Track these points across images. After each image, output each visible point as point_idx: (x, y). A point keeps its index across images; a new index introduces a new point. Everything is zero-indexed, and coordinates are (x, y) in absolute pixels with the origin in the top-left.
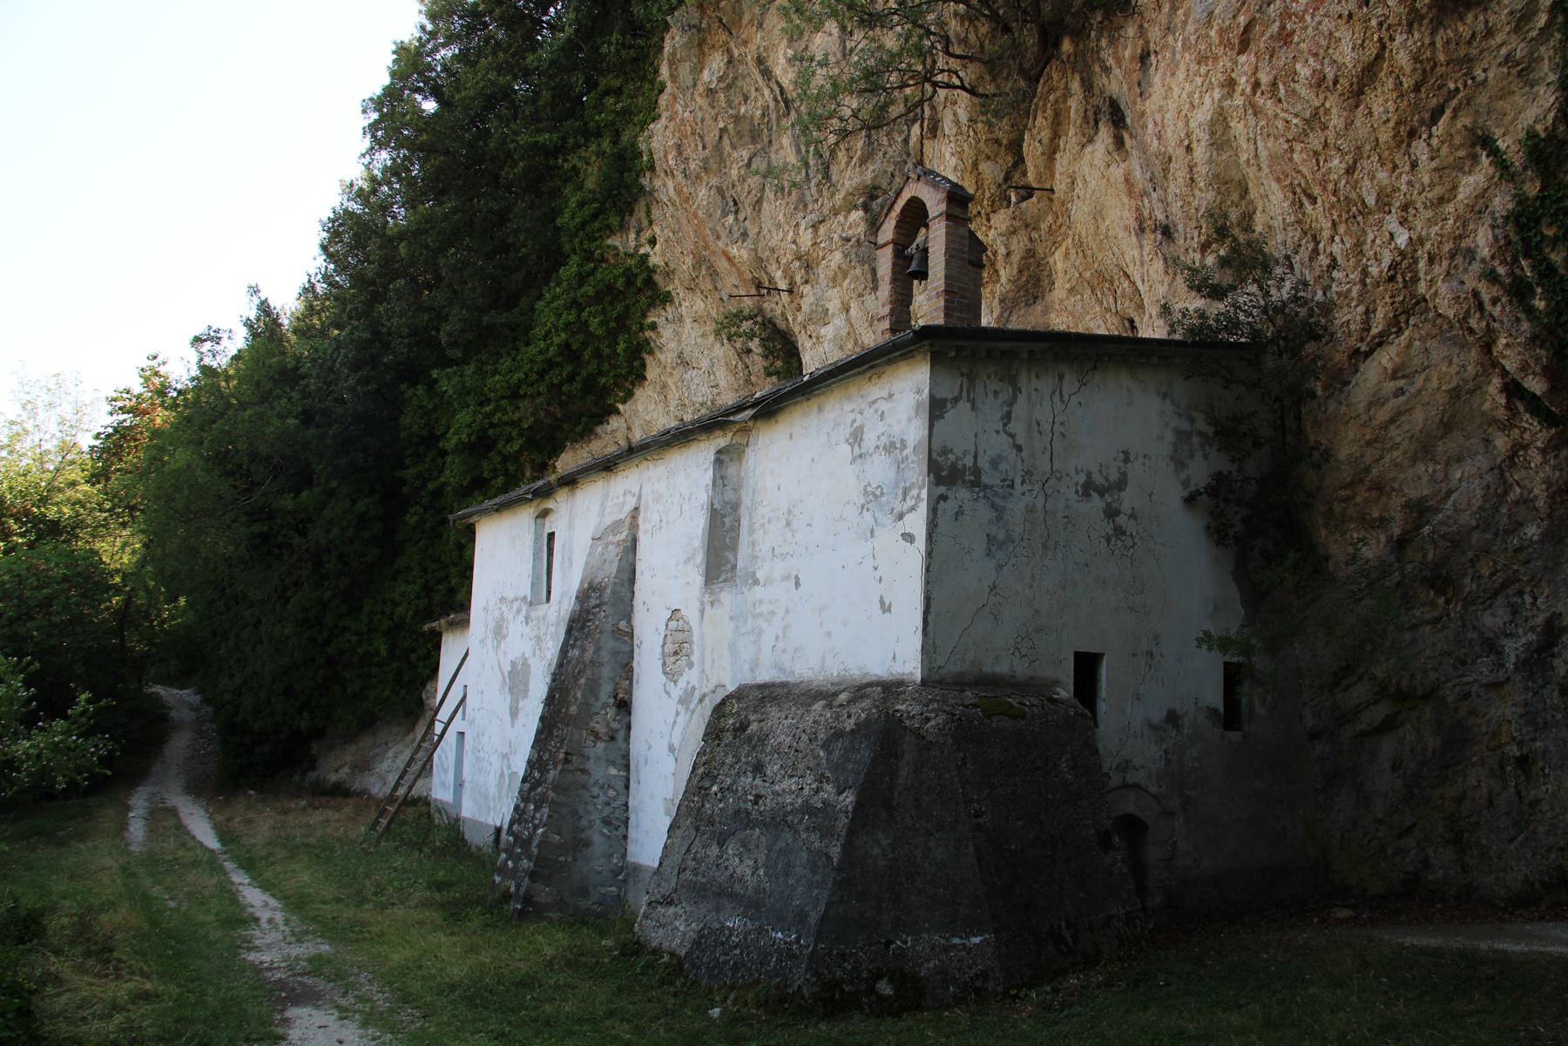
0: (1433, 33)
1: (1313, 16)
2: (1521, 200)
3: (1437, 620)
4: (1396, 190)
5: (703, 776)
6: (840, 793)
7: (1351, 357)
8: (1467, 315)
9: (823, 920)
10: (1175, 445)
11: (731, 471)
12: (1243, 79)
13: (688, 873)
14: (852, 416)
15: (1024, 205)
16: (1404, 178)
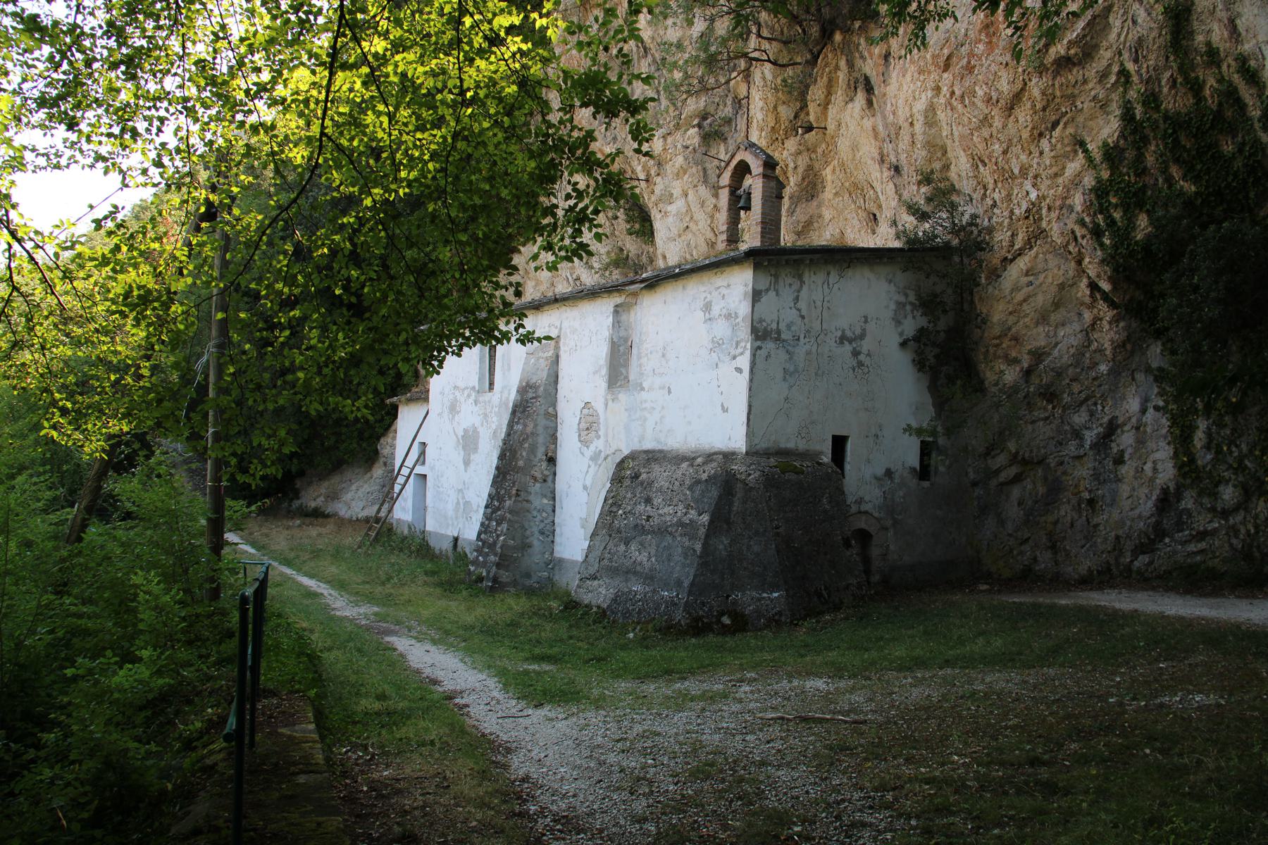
0: (1054, 79)
1: (986, 59)
2: (1099, 180)
3: (1047, 418)
4: (1031, 166)
5: (612, 505)
6: (700, 515)
7: (1002, 262)
8: (1068, 243)
9: (692, 584)
10: (895, 311)
11: (624, 317)
12: (945, 89)
13: (606, 561)
14: (704, 295)
15: (807, 136)
16: (1036, 160)
